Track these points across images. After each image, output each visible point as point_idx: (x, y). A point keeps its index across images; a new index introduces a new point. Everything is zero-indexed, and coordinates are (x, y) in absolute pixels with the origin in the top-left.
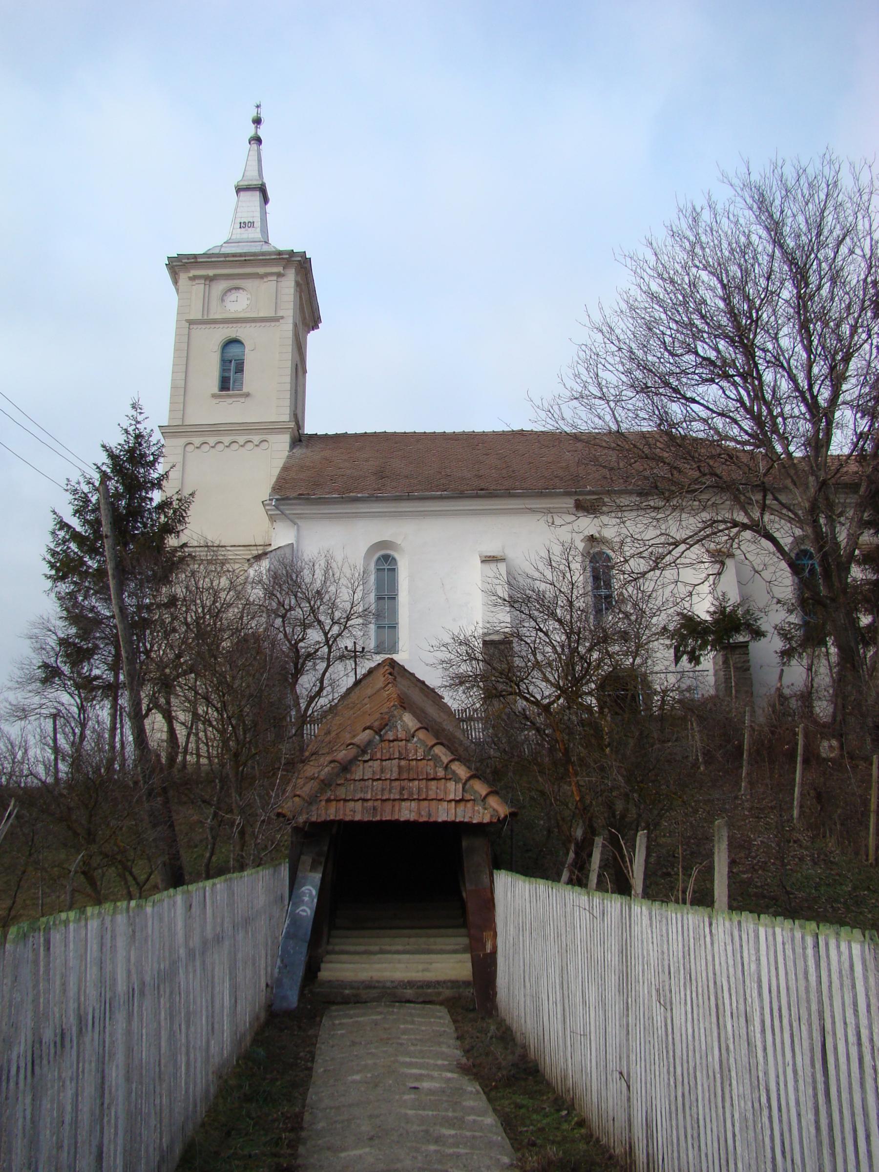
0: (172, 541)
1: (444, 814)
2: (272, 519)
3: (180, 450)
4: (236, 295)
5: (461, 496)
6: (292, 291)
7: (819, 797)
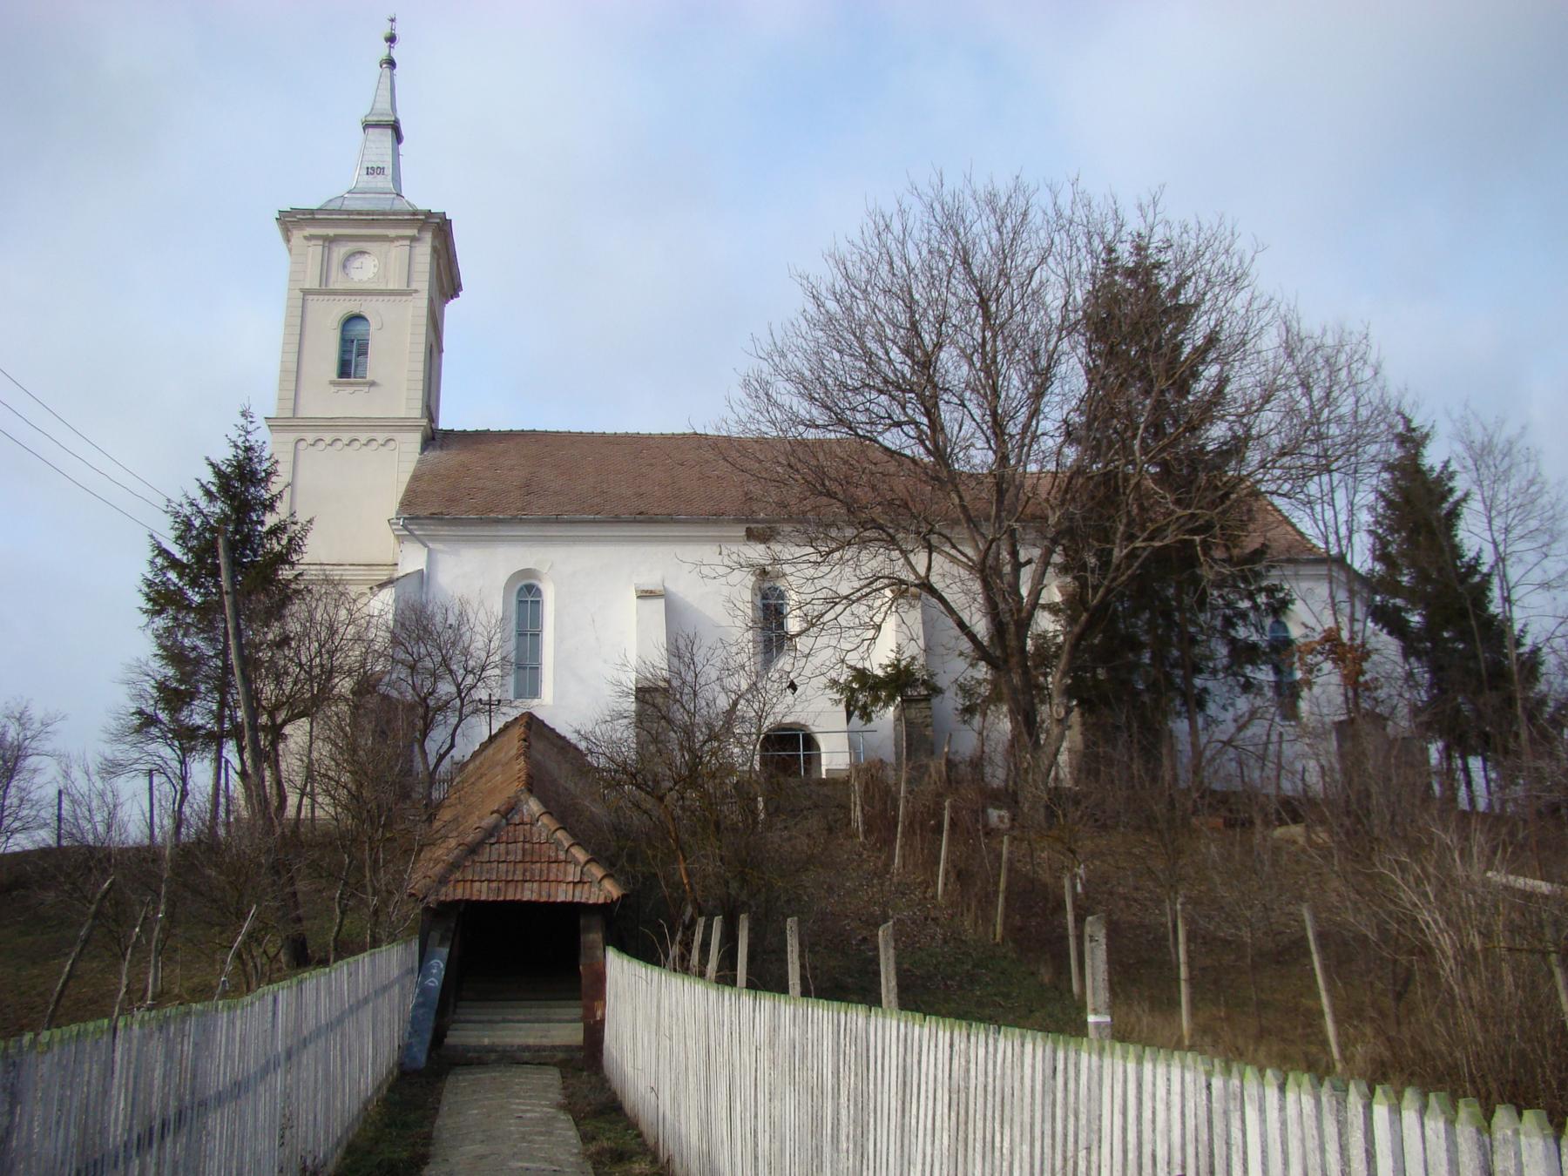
0: (286, 573)
1: (563, 894)
2: (400, 539)
3: (291, 447)
5: (617, 520)
6: (428, 259)
7: (959, 875)
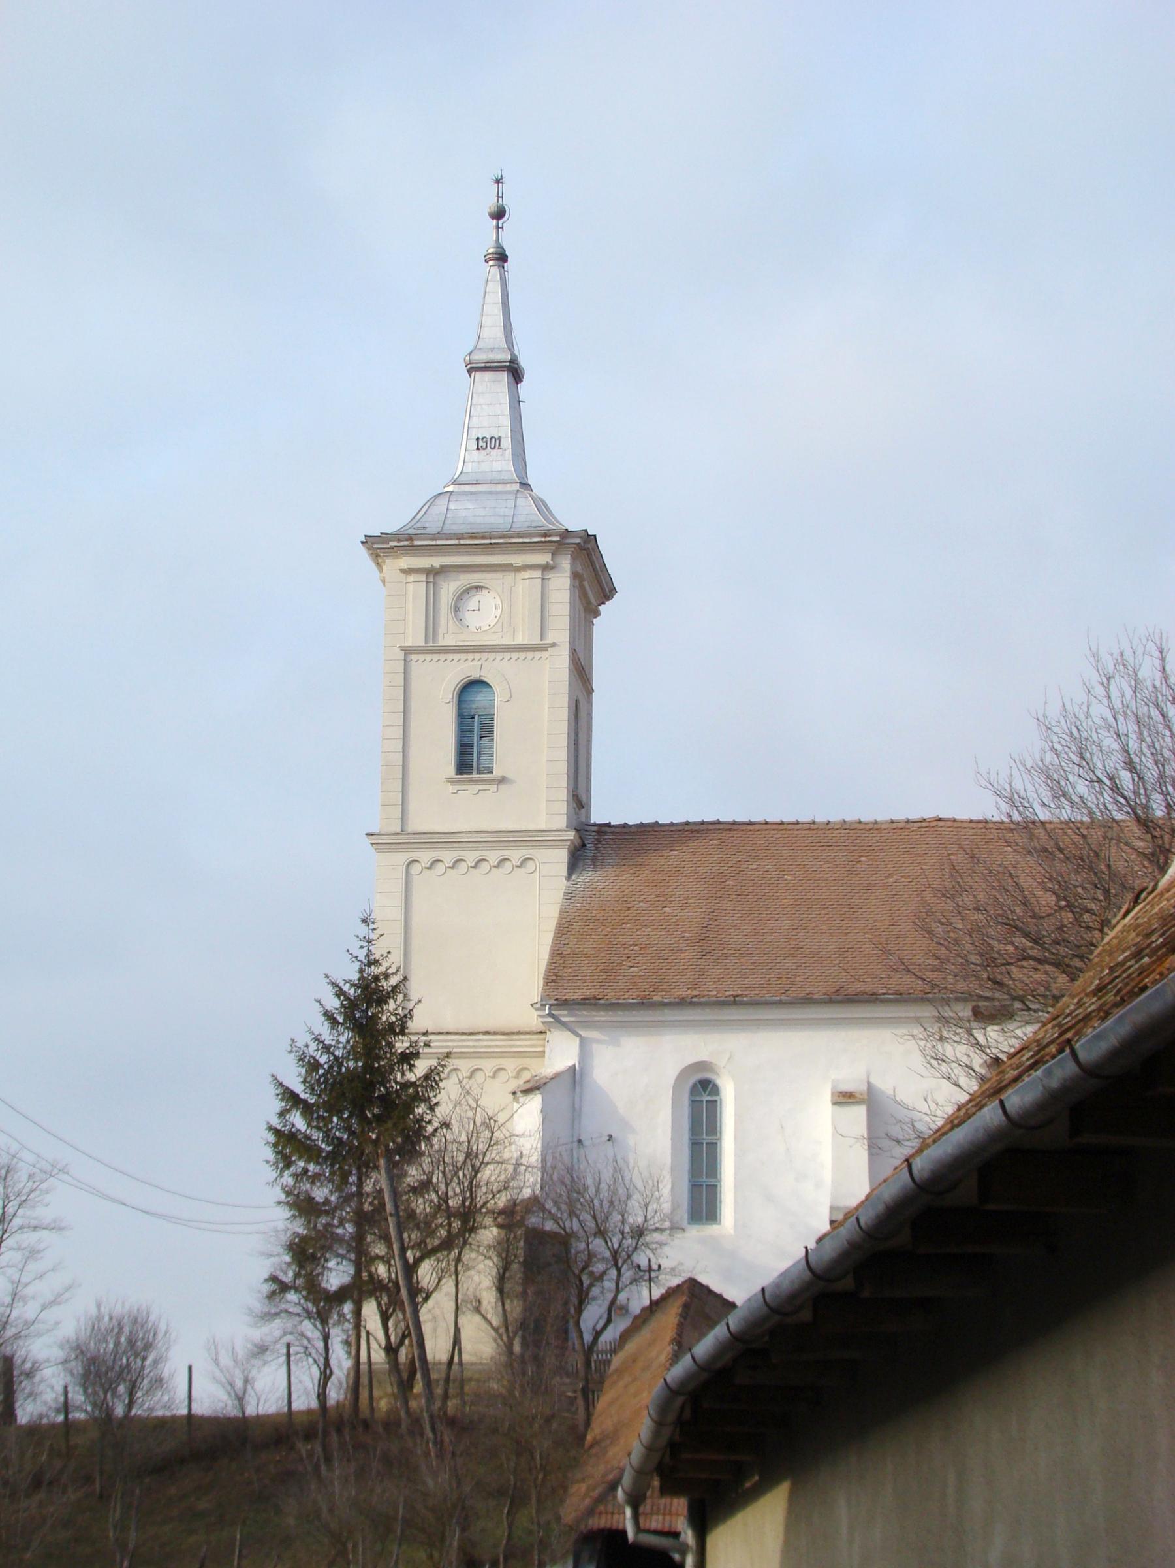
3: (400, 873)
4: (477, 598)
5: (808, 1001)
